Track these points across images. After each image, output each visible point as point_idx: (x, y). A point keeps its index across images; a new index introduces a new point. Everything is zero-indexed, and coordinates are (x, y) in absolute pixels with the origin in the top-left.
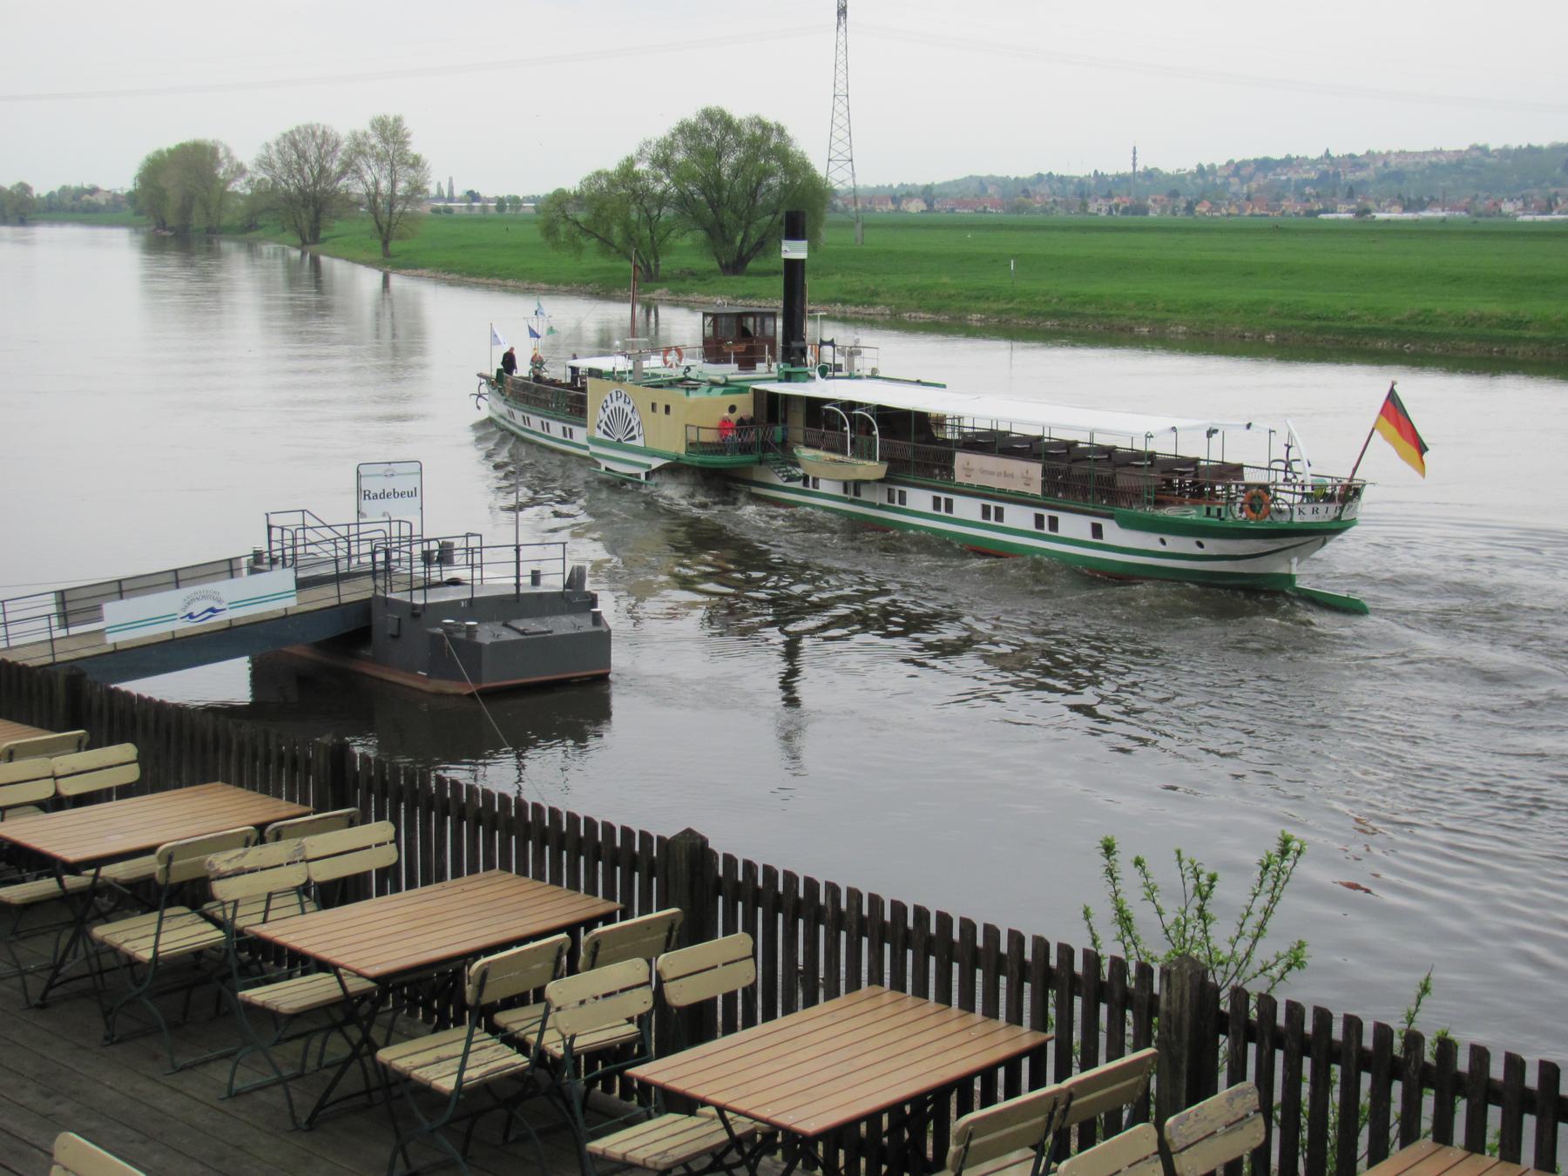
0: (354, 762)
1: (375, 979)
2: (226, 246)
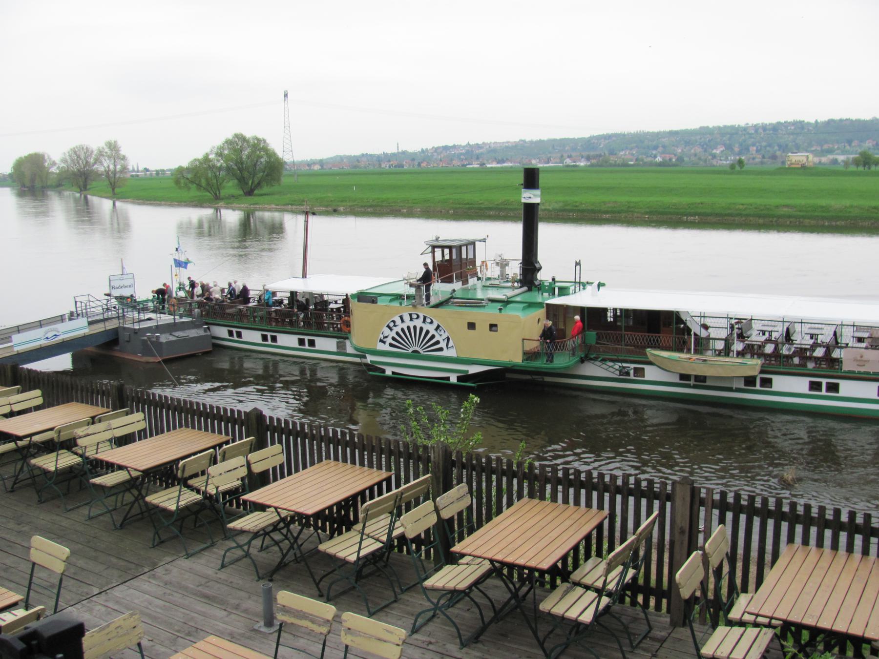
0: (265, 421)
1: (143, 471)
2: (49, 193)
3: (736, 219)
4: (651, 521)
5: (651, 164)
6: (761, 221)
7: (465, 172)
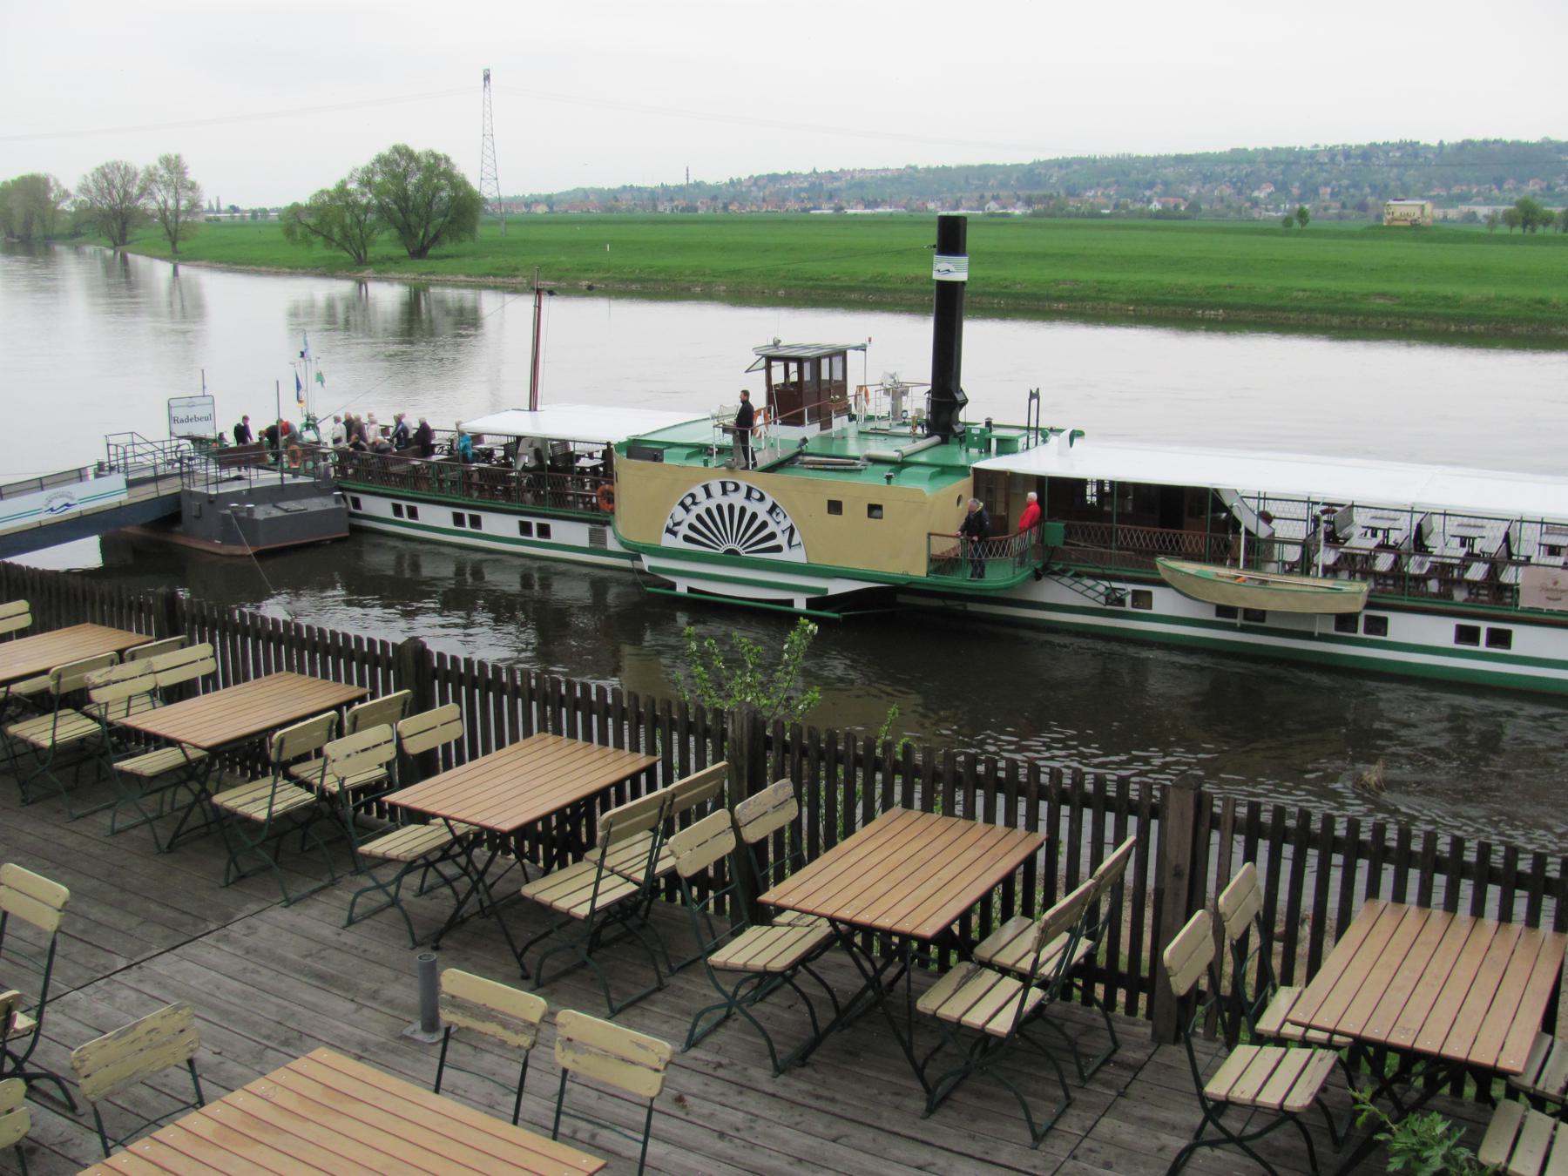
0: (431, 660)
2: (58, 248)
7: (809, 222)
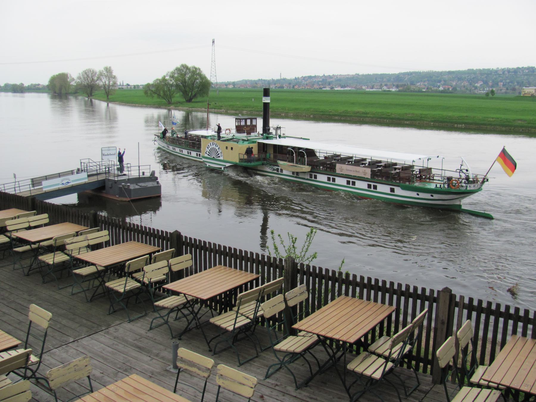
0: (182, 239)
2: (71, 97)
3: (488, 127)
4: (424, 314)
5: (436, 91)
6: (504, 129)
